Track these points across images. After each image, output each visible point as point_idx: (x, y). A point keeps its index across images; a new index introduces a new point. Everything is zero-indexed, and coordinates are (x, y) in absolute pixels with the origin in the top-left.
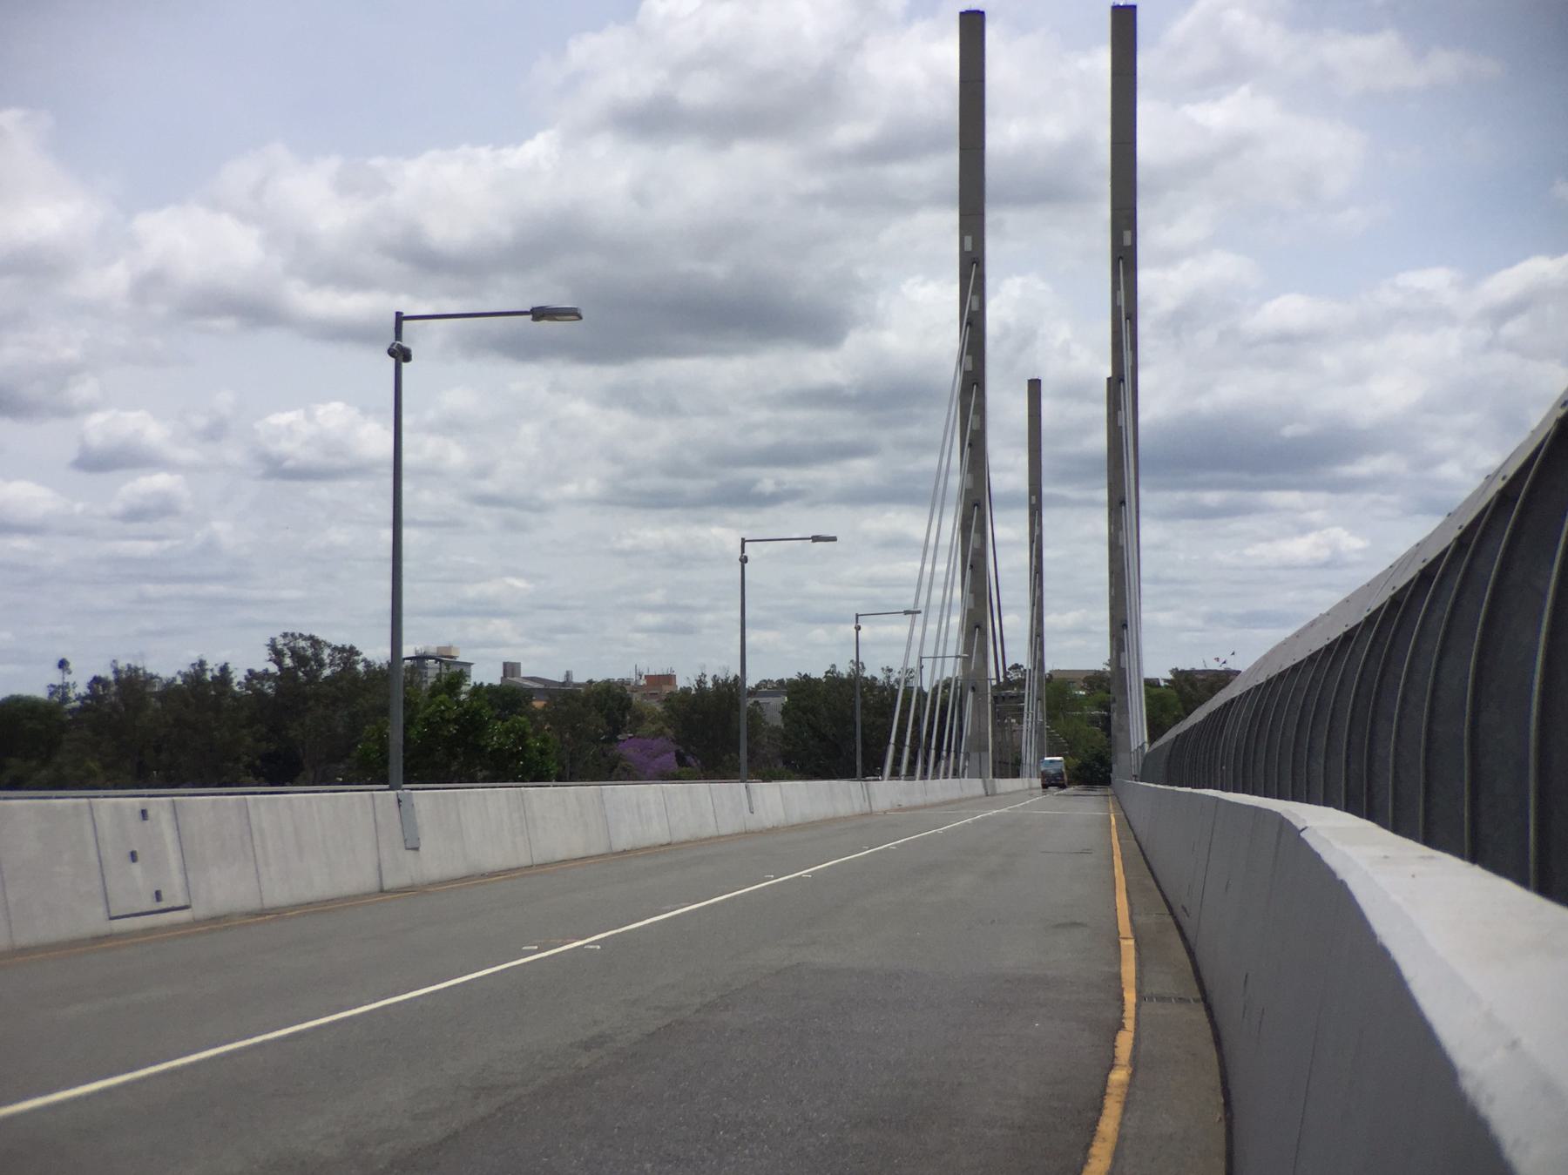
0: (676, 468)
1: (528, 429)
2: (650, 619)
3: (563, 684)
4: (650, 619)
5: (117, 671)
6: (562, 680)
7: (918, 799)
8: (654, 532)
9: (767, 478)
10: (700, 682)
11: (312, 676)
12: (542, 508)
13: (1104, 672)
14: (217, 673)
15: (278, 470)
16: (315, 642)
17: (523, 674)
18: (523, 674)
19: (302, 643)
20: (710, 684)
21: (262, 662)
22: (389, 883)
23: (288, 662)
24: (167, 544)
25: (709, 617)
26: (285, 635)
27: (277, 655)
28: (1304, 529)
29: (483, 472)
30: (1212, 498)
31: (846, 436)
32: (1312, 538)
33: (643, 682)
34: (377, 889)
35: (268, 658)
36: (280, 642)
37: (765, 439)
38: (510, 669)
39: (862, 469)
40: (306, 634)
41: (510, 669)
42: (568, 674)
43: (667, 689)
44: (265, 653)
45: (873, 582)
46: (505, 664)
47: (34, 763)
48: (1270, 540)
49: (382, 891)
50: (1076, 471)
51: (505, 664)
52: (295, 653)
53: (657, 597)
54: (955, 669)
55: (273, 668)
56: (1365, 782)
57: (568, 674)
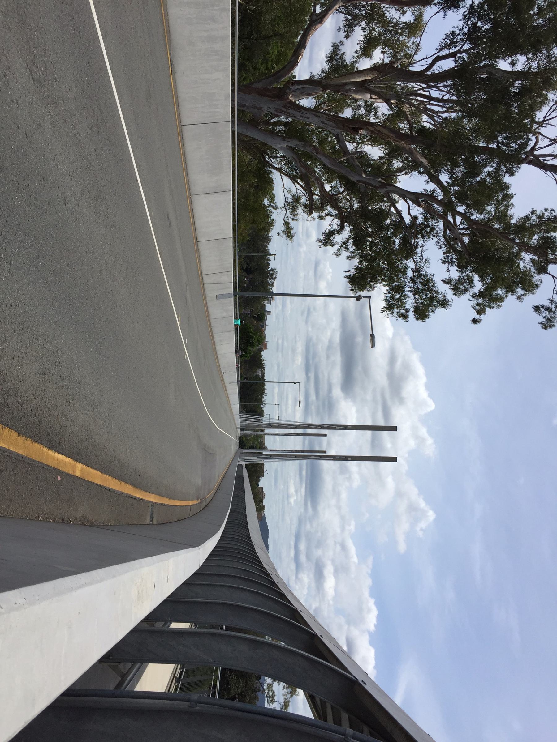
0: (315, 355)
1: (324, 321)
2: (280, 342)
3: (265, 324)
4: (280, 342)
5: (270, 236)
6: (266, 324)
7: (226, 378)
8: (300, 347)
9: (312, 375)
10: (264, 360)
11: (267, 277)
12: (306, 322)
13: (264, 445)
14: (269, 258)
15: (317, 264)
16: (275, 278)
17: (268, 315)
18: (268, 315)
19: (275, 275)
20: (263, 362)
21: (271, 266)
22: (205, 285)
23: (271, 272)
24: (301, 236)
25: (280, 355)
26: (277, 272)
27: (272, 270)
28: (296, 491)
29: (315, 309)
30: (304, 473)
31: (321, 393)
32: (294, 493)
33: (265, 342)
34: (204, 283)
35: (271, 237)
36: (275, 271)
37: (321, 376)
38: (269, 312)
39: (313, 397)
40: (277, 276)
41: (269, 312)
42: (267, 325)
43: (263, 348)
44: (273, 268)
45: (287, 397)
46: (270, 311)
47: (251, 334)
48: (294, 484)
49: (203, 284)
50: (311, 443)
51: (270, 311)
52: (273, 274)
53: (285, 344)
54: (266, 421)
55: (270, 269)
56: (169, 56)
57: (267, 325)
